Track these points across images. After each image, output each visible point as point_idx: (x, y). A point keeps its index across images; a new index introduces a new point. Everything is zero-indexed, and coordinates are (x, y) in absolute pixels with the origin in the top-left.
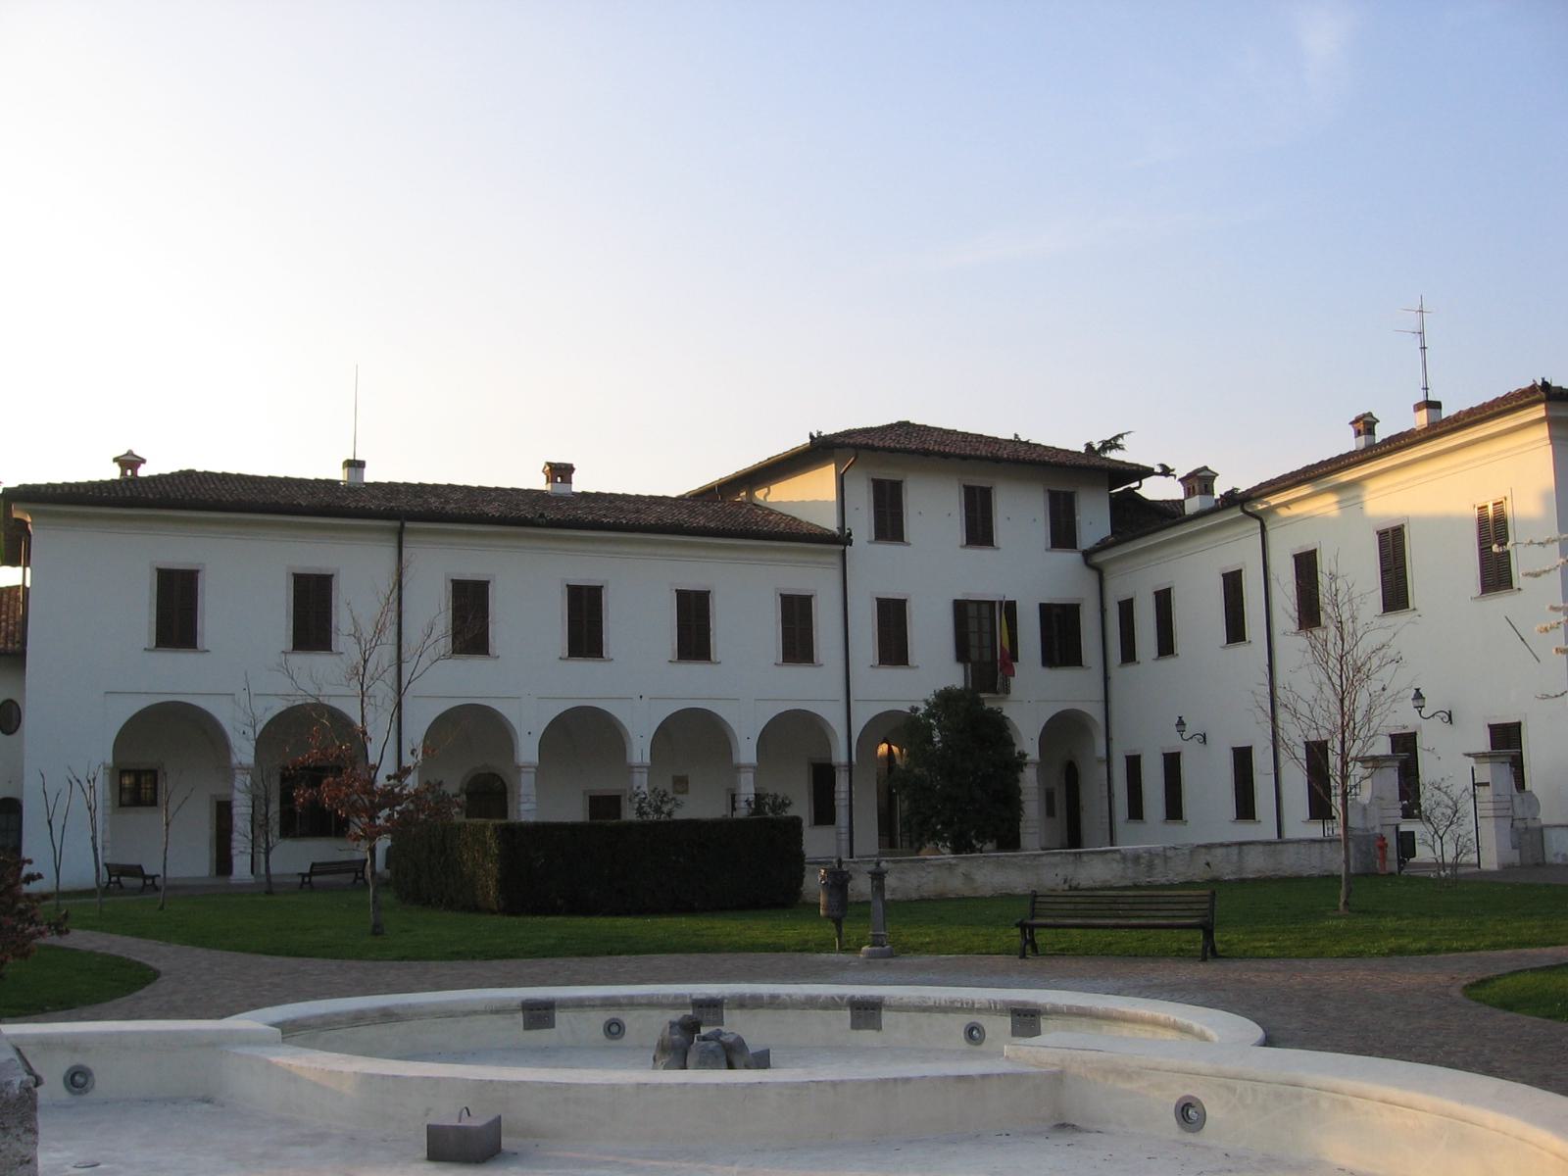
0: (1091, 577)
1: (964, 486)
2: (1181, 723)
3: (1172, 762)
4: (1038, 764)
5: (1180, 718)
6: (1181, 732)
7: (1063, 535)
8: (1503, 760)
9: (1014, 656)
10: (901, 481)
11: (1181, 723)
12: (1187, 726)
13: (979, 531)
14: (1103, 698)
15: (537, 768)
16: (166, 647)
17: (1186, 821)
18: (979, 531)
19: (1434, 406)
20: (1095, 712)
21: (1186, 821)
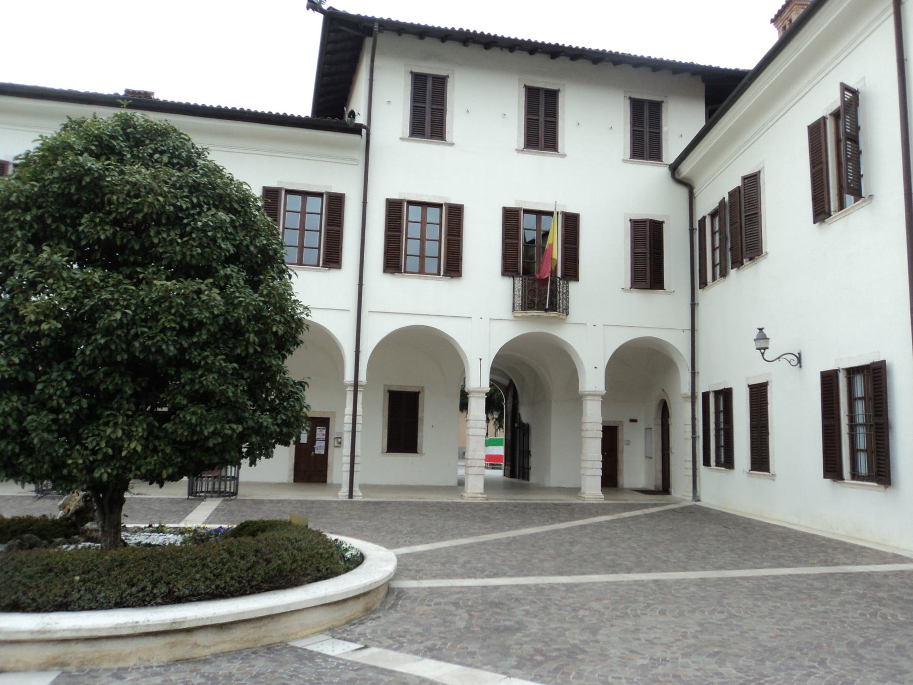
0: (683, 192)
1: (525, 86)
2: (762, 336)
3: (759, 394)
4: (603, 397)
5: (761, 330)
6: (763, 349)
7: (645, 143)
8: (596, 398)
9: (571, 270)
10: (448, 76)
11: (762, 336)
12: (771, 341)
13: (541, 132)
14: (689, 327)
15: (603, 397)
16: (886, 399)
17: (871, 196)
18: (541, 132)
19: (564, 673)
20: (679, 343)
21: (871, 196)
